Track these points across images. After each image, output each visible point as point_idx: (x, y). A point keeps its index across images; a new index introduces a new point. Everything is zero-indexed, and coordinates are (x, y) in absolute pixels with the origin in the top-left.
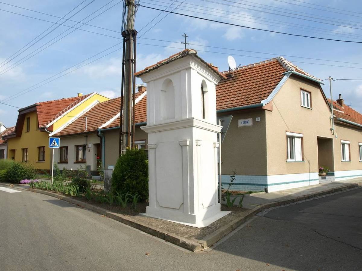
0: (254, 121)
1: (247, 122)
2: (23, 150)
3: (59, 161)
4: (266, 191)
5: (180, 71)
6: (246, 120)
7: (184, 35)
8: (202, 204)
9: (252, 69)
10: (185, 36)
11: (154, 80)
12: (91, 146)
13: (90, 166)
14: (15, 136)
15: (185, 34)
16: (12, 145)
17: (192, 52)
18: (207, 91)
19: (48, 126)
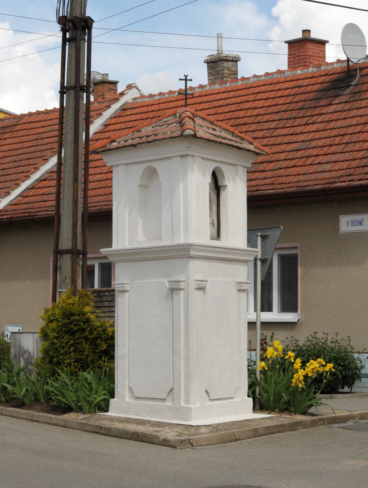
5: (170, 158)
6: (358, 217)
7: (184, 78)
8: (206, 391)
10: (186, 80)
11: (127, 164)
15: (186, 75)
17: (188, 133)
18: (224, 184)
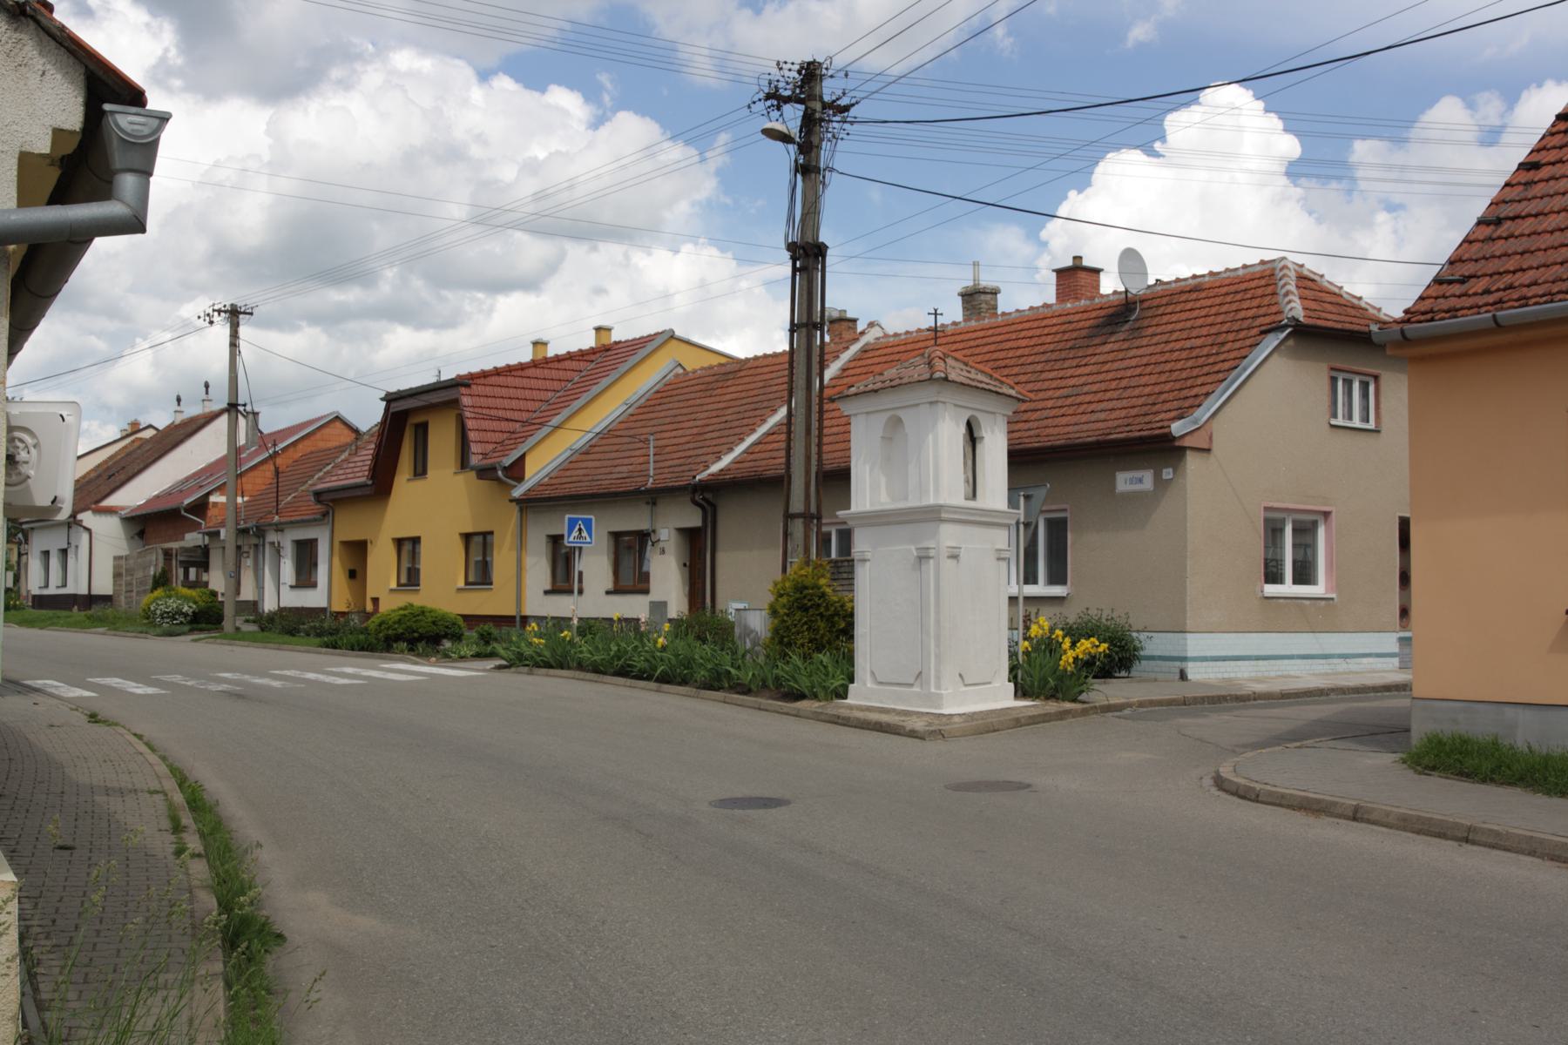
0: (1157, 478)
1: (1140, 481)
2: (399, 542)
3: (548, 587)
4: (1183, 676)
9: (1194, 296)
12: (666, 534)
13: (664, 604)
14: (367, 491)
16: (350, 526)
19: (507, 462)
